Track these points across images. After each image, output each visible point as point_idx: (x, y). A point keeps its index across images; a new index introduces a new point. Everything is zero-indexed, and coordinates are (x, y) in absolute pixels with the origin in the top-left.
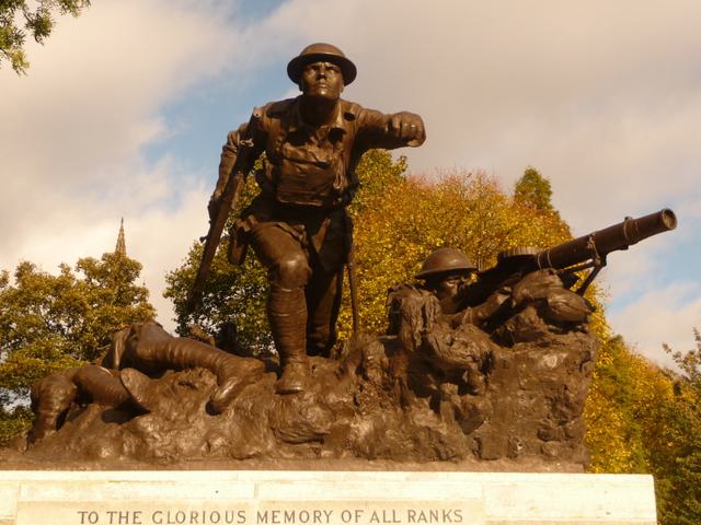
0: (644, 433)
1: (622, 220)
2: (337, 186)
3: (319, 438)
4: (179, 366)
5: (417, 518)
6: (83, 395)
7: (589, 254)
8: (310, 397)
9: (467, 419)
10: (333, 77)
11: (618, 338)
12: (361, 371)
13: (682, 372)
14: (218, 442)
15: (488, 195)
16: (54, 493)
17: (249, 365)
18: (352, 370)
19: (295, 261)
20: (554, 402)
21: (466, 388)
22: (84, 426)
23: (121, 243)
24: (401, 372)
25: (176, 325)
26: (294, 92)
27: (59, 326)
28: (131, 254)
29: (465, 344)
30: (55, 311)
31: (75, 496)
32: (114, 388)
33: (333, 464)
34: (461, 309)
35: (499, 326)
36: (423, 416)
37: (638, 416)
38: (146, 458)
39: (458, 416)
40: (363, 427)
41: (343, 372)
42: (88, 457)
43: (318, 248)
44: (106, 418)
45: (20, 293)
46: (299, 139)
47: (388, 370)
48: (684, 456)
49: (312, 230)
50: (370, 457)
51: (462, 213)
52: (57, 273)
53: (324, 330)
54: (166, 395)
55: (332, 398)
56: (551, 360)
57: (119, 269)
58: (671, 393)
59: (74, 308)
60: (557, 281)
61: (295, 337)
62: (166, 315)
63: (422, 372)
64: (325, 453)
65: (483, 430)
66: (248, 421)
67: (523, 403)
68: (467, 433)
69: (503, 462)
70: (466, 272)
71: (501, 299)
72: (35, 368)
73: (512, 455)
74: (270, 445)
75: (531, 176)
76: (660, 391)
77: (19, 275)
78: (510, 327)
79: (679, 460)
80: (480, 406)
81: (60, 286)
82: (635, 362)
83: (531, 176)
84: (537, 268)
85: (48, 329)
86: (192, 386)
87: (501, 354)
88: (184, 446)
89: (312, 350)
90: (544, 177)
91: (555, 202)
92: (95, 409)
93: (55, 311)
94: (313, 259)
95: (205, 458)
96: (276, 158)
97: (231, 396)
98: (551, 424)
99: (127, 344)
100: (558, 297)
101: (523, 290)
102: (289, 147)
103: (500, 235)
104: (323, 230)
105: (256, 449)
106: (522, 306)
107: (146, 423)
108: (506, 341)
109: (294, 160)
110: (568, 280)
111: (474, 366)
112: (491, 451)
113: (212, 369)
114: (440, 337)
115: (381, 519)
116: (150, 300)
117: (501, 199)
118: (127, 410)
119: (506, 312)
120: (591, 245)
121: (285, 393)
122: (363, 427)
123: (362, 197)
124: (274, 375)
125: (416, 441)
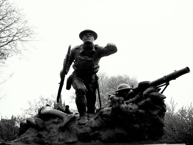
26: (81, 42)
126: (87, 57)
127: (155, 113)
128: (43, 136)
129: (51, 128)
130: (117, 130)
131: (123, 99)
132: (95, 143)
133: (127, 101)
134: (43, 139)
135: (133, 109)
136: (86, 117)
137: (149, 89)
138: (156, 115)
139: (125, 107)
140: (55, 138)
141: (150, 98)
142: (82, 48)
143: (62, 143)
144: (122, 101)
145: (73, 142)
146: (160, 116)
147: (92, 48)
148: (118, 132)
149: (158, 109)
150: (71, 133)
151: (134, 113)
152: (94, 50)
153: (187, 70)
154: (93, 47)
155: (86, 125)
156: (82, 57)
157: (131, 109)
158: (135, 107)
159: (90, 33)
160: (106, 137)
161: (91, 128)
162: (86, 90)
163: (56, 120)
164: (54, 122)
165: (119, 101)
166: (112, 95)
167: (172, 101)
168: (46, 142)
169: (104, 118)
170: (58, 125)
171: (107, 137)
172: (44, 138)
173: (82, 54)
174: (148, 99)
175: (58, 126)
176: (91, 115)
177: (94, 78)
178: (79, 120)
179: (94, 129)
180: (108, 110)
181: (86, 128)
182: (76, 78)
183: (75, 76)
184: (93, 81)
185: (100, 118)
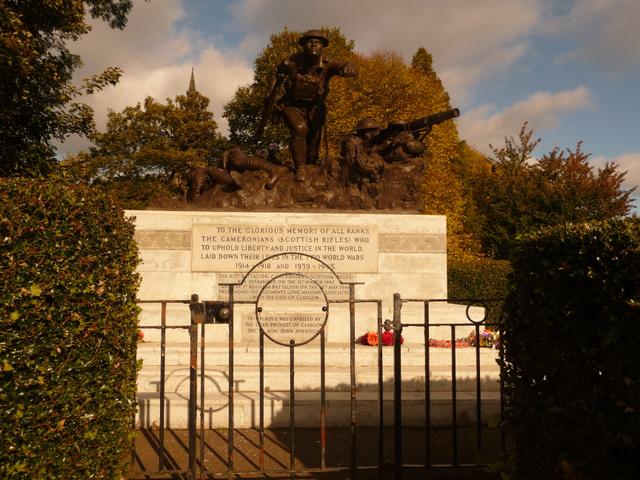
0: (474, 192)
2: (320, 93)
3: (312, 200)
4: (252, 169)
6: (212, 181)
7: (424, 125)
8: (308, 183)
9: (372, 193)
10: (319, 46)
11: (464, 142)
12: (329, 172)
13: (498, 160)
14: (270, 201)
15: (397, 64)
16: (208, 220)
17: (282, 169)
18: (326, 173)
19: (302, 126)
20: (408, 186)
21: (372, 180)
22: (214, 193)
23: (192, 82)
24: (346, 173)
25: (230, 133)
27: (167, 133)
29: (373, 162)
30: (165, 124)
31: (215, 221)
32: (226, 177)
33: (317, 210)
34: (372, 146)
35: (387, 154)
36: (355, 192)
37: (473, 184)
38: (241, 207)
39: (369, 191)
40: (330, 196)
41: (321, 173)
42: (218, 206)
43: (311, 118)
44: (224, 190)
45: (146, 114)
46: (304, 72)
47: (340, 172)
48: (495, 203)
49: (308, 111)
50: (333, 207)
51: (383, 75)
52: (165, 104)
53: (313, 153)
54: (248, 181)
55: (317, 184)
56: (408, 169)
58: (490, 172)
59: (175, 123)
60: (412, 136)
61: (301, 158)
62: (223, 129)
63: (354, 174)
64: (314, 206)
65: (379, 196)
66: (282, 193)
67: (396, 186)
68: (373, 198)
69: (387, 210)
70: (375, 129)
71: (389, 142)
72: (155, 155)
73: (391, 207)
74: (292, 202)
75: (422, 51)
76: (485, 170)
77: (146, 104)
78: (392, 156)
79: (493, 205)
80: (378, 187)
81: (166, 111)
82: (471, 153)
83: (422, 51)
84: (403, 130)
85: (160, 134)
86: (259, 178)
87: (387, 166)
88: (256, 202)
89: (308, 163)
90: (429, 52)
91: (434, 67)
92: (218, 187)
93: (165, 124)
94: (309, 124)
95: (266, 207)
96: (294, 80)
97: (276, 182)
98: (407, 195)
99: (228, 158)
100: (412, 143)
101: (397, 140)
102: (299, 75)
103: (403, 87)
104: (313, 111)
105: (286, 204)
106: (396, 147)
107: (241, 193)
108: (389, 161)
109: (301, 81)
110: (416, 136)
111: (376, 171)
112: (382, 206)
113: (267, 170)
114: (362, 159)
116: (214, 119)
117: (404, 67)
118: (232, 188)
119: (390, 149)
120: (426, 121)
121: (298, 181)
122: (330, 196)
123: (329, 97)
124: (292, 173)
125: (352, 202)
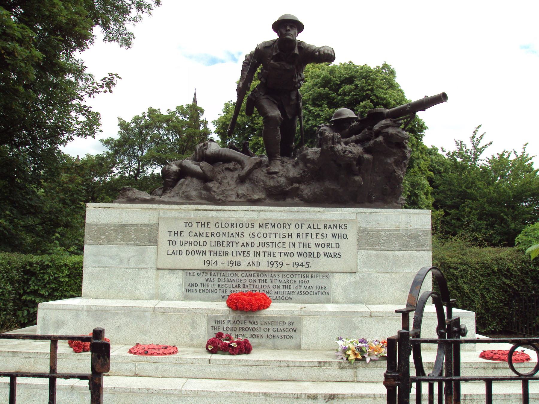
1: (423, 97)
5: (327, 227)
16: (174, 214)
23: (195, 100)
26: (275, 36)
28: (199, 105)
31: (183, 215)
57: (194, 111)
81: (167, 120)
115: (312, 227)
126: (283, 63)
127: (389, 161)
128: (214, 189)
129: (224, 178)
130: (328, 185)
131: (339, 136)
132: (367, 92)
133: (347, 139)
134: (213, 193)
135: (354, 153)
136: (279, 162)
137: (383, 122)
138: (391, 164)
139: (342, 149)
140: (230, 193)
141: (383, 136)
142: (276, 48)
143: (242, 200)
144: (338, 139)
145: (259, 199)
146: (397, 166)
147: (293, 49)
148: (329, 187)
149: (394, 154)
150: (256, 185)
151: (354, 158)
152: (296, 51)
153: (442, 98)
154: (295, 46)
155: (280, 174)
156: (275, 63)
157: (350, 152)
158: (357, 149)
159: (291, 24)
160: (309, 194)
161: (287, 178)
162: (280, 118)
163: (231, 165)
164: (228, 169)
165: (333, 138)
166: (323, 126)
167: (478, 136)
168: (218, 198)
169: (308, 165)
170: (234, 174)
171: (311, 194)
172: (214, 192)
173: (277, 58)
174: (380, 138)
175: (236, 174)
176: (285, 159)
177: (294, 97)
178: (267, 166)
179: (291, 180)
180: (316, 153)
181: (279, 179)
182: (264, 97)
183: (263, 94)
184: (292, 103)
185: (301, 165)
